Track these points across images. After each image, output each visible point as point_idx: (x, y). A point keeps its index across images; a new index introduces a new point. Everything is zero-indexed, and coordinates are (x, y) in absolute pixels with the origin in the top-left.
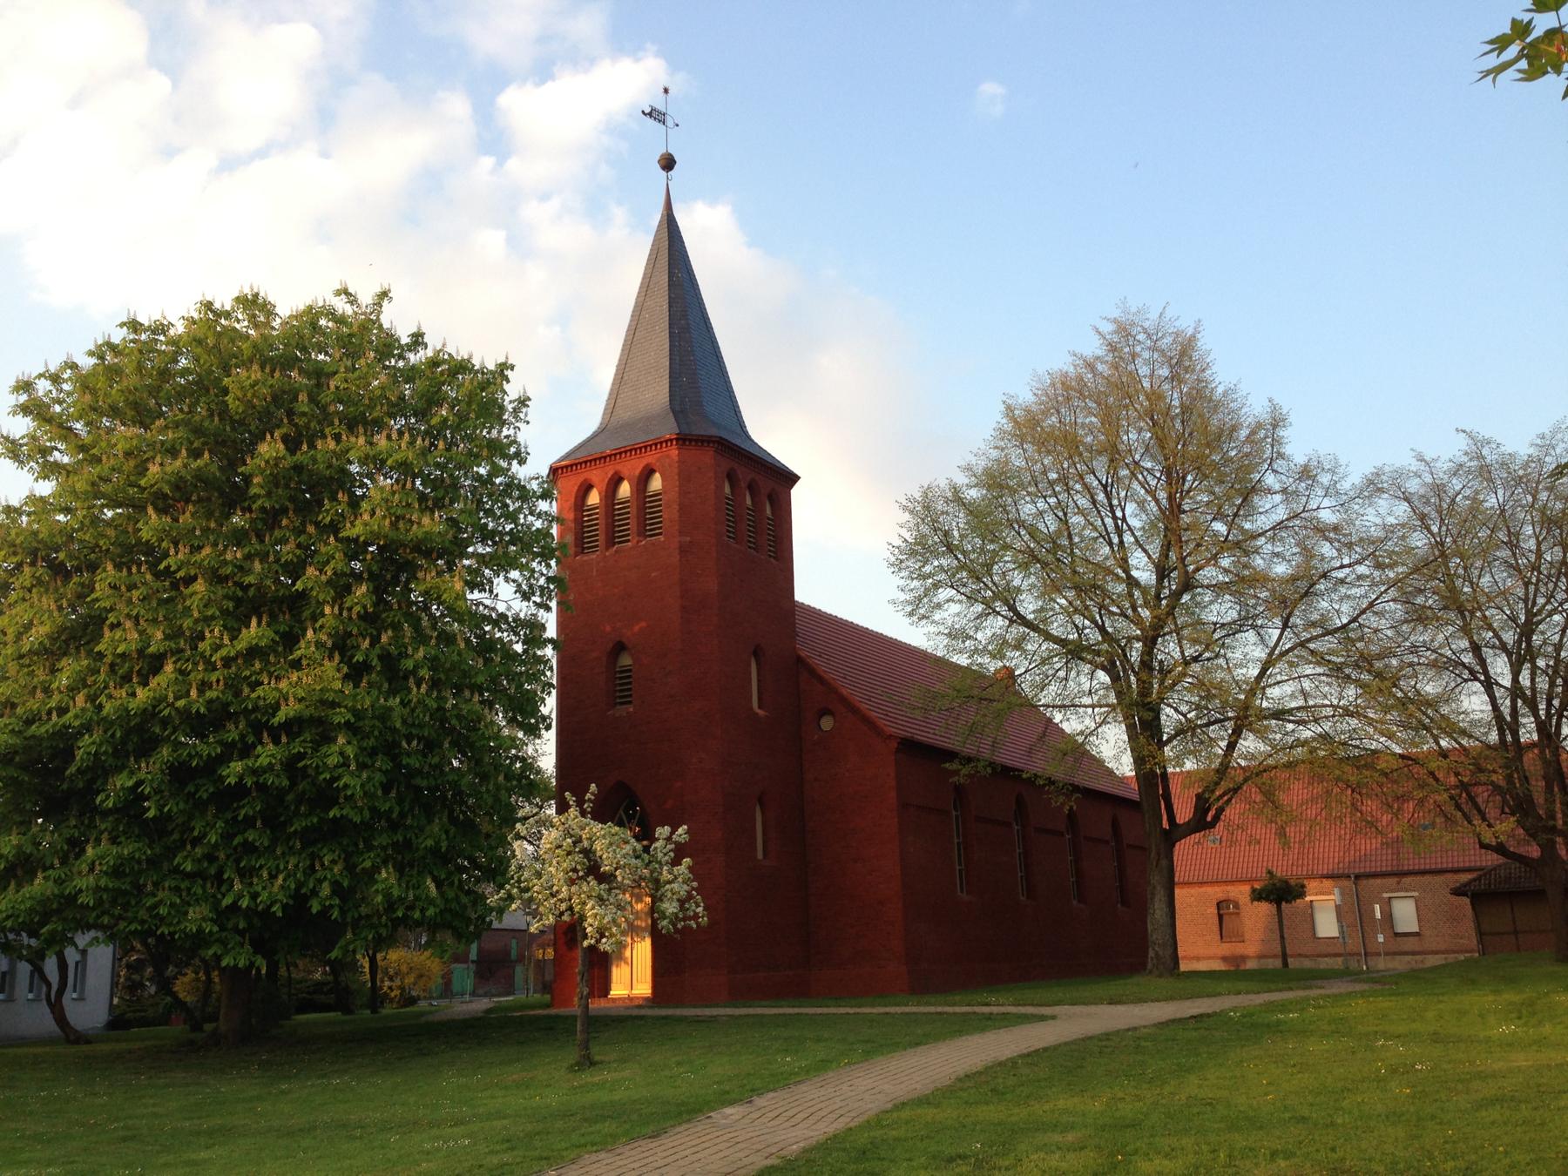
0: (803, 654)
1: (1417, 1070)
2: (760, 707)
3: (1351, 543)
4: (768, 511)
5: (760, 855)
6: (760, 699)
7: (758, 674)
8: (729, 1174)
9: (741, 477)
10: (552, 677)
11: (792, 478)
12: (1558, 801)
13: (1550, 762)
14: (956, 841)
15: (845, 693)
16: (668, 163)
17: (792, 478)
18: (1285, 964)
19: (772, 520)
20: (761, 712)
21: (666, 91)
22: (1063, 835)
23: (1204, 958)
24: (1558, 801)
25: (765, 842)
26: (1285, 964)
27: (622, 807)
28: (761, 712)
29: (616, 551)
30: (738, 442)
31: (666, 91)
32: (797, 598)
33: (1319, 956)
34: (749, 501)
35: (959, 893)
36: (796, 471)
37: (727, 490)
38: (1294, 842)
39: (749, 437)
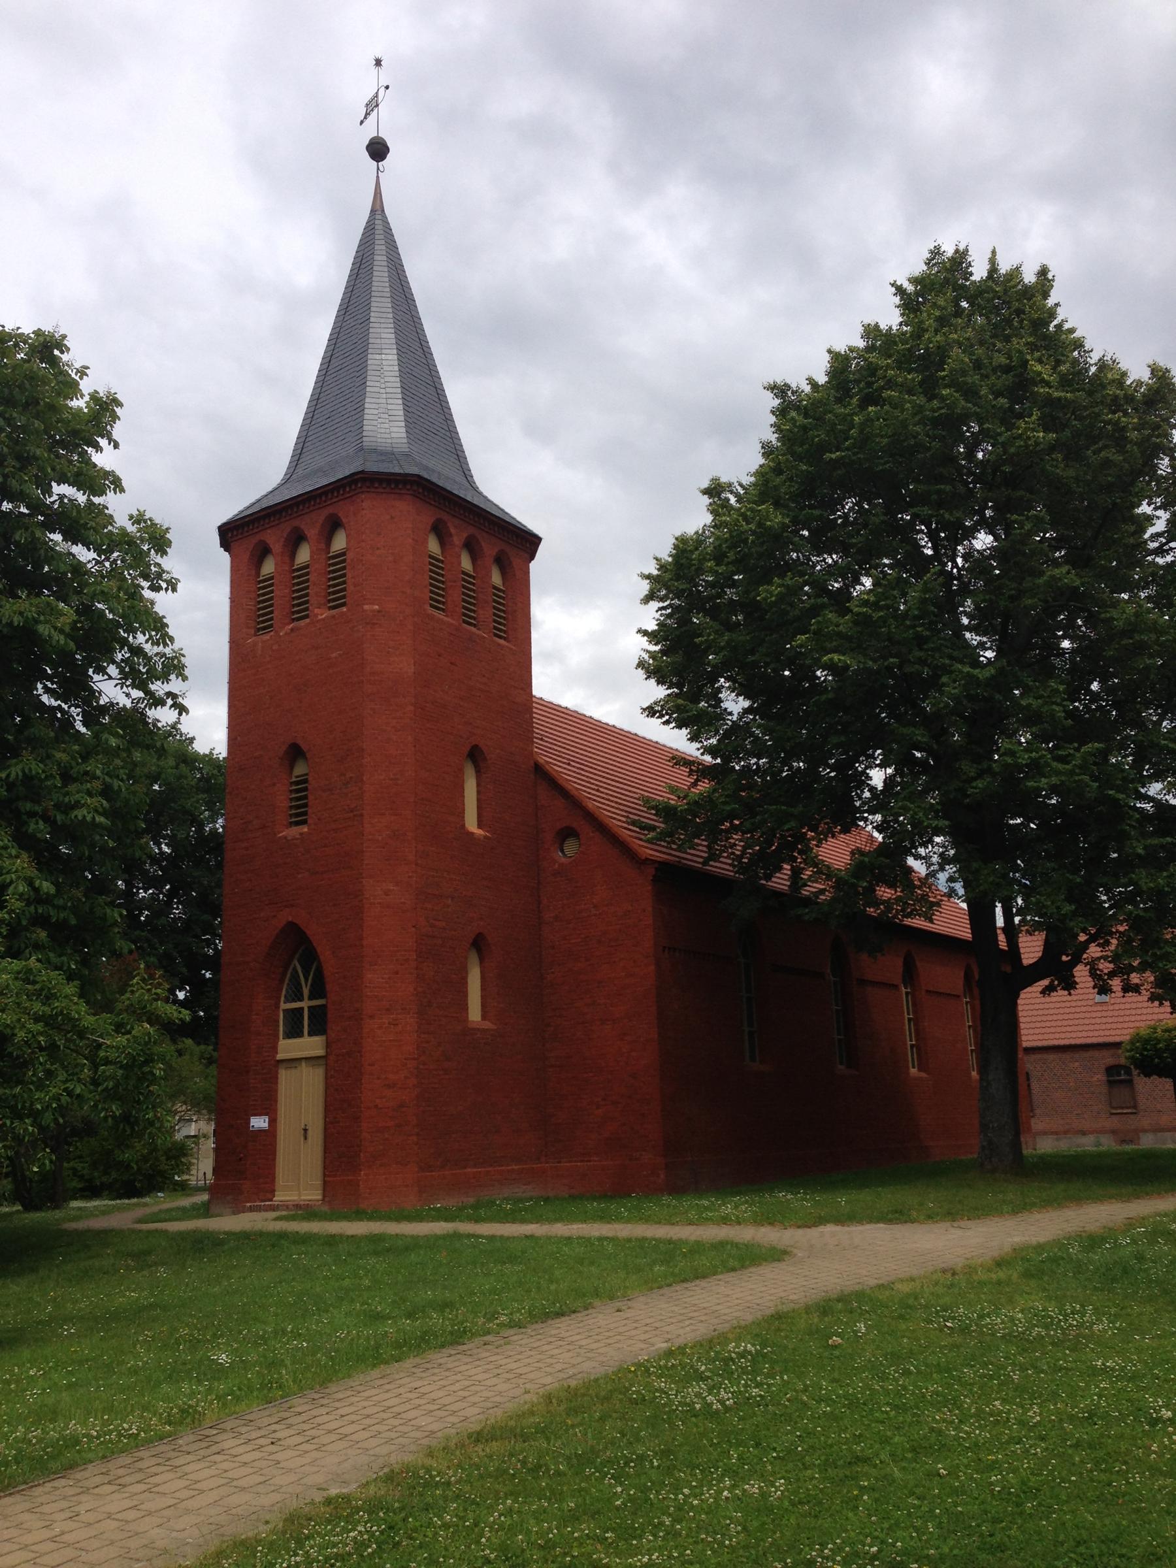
0: (542, 759)
1: (613, 1530)
2: (480, 826)
11: (528, 542)
12: (1062, 394)
14: (906, 1016)
15: (590, 806)
17: (528, 542)
19: (503, 592)
21: (378, 62)
22: (896, 987)
23: (1092, 1133)
24: (1062, 394)
27: (297, 956)
29: (292, 630)
30: (476, 501)
31: (378, 62)
32: (534, 693)
36: (540, 535)
38: (884, 892)
39: (480, 493)
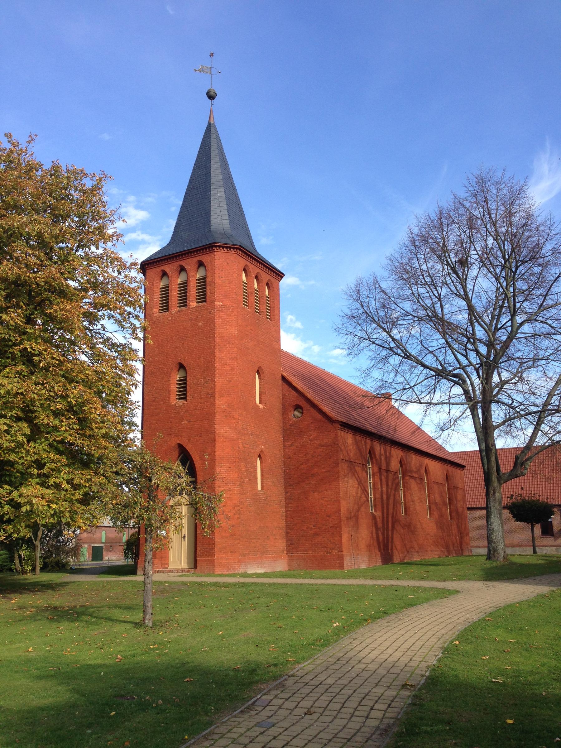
3: (72, 486)
4: (267, 293)
5: (259, 488)
6: (260, 398)
7: (260, 384)
8: (227, 746)
9: (251, 270)
10: (139, 377)
13: (127, 434)
16: (211, 96)
18: (535, 552)
20: (261, 406)
25: (262, 480)
26: (535, 552)
28: (261, 406)
32: (282, 348)
33: (543, 546)
34: (256, 286)
35: (174, 401)
37: (244, 278)
